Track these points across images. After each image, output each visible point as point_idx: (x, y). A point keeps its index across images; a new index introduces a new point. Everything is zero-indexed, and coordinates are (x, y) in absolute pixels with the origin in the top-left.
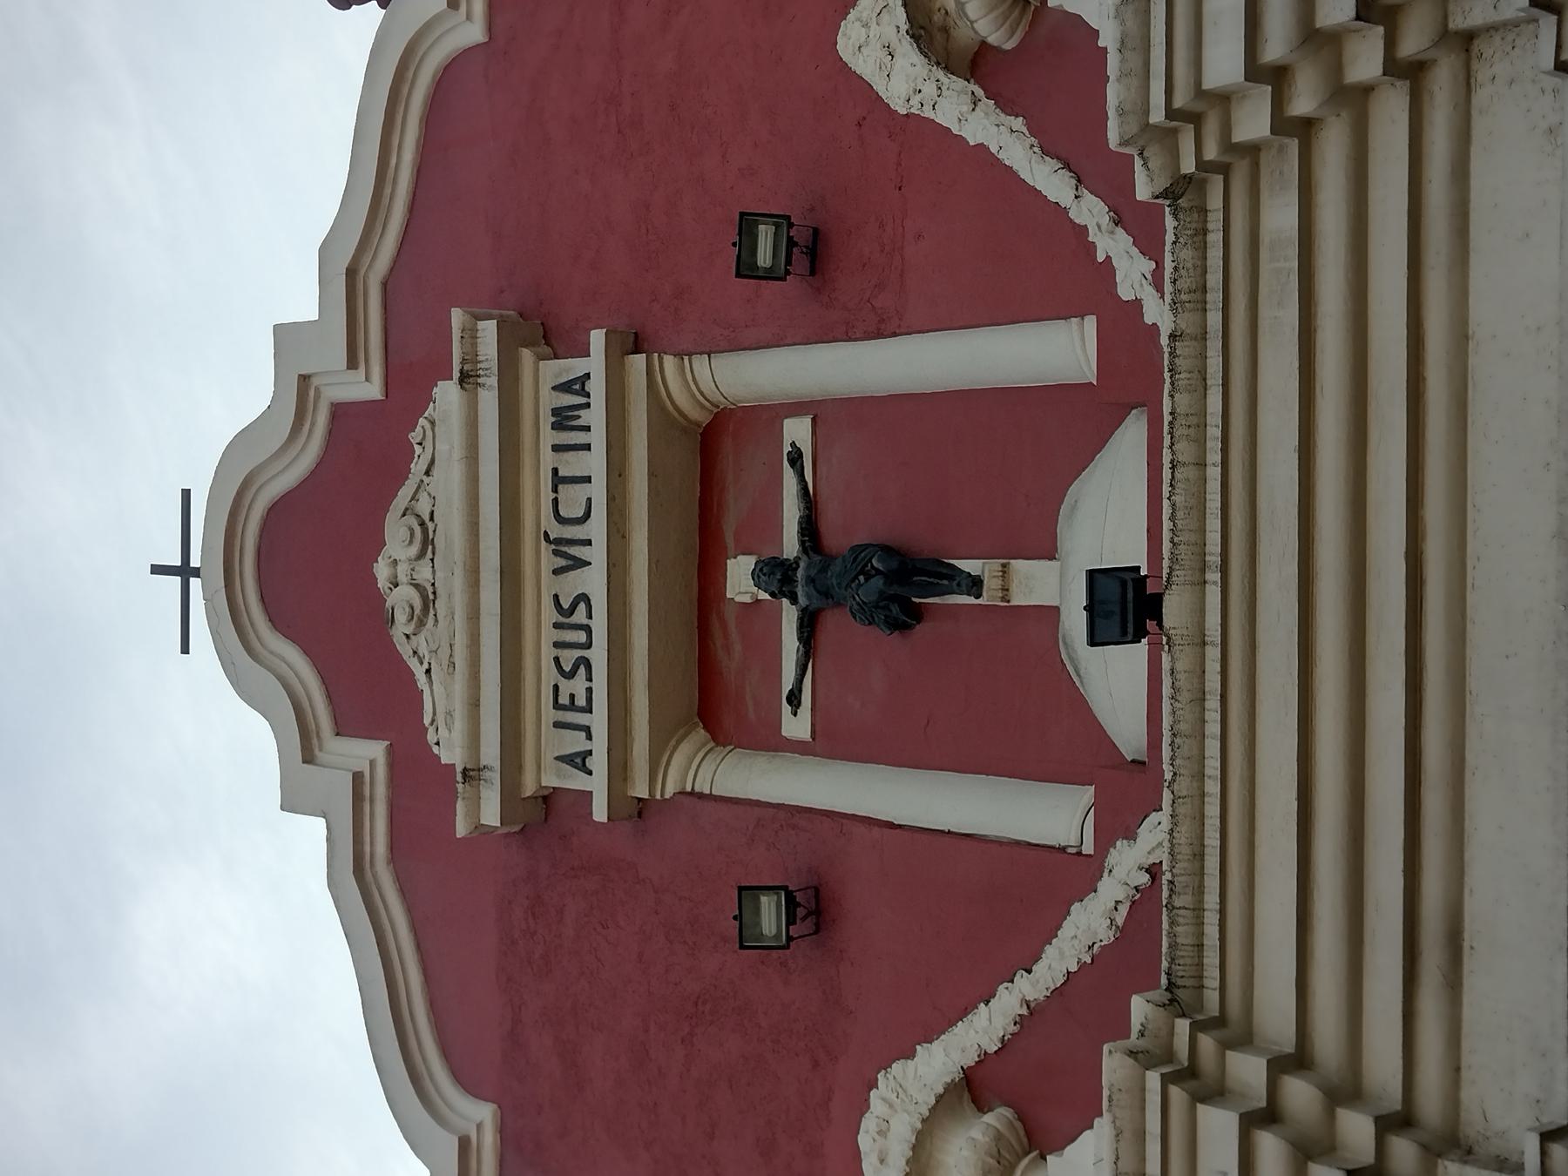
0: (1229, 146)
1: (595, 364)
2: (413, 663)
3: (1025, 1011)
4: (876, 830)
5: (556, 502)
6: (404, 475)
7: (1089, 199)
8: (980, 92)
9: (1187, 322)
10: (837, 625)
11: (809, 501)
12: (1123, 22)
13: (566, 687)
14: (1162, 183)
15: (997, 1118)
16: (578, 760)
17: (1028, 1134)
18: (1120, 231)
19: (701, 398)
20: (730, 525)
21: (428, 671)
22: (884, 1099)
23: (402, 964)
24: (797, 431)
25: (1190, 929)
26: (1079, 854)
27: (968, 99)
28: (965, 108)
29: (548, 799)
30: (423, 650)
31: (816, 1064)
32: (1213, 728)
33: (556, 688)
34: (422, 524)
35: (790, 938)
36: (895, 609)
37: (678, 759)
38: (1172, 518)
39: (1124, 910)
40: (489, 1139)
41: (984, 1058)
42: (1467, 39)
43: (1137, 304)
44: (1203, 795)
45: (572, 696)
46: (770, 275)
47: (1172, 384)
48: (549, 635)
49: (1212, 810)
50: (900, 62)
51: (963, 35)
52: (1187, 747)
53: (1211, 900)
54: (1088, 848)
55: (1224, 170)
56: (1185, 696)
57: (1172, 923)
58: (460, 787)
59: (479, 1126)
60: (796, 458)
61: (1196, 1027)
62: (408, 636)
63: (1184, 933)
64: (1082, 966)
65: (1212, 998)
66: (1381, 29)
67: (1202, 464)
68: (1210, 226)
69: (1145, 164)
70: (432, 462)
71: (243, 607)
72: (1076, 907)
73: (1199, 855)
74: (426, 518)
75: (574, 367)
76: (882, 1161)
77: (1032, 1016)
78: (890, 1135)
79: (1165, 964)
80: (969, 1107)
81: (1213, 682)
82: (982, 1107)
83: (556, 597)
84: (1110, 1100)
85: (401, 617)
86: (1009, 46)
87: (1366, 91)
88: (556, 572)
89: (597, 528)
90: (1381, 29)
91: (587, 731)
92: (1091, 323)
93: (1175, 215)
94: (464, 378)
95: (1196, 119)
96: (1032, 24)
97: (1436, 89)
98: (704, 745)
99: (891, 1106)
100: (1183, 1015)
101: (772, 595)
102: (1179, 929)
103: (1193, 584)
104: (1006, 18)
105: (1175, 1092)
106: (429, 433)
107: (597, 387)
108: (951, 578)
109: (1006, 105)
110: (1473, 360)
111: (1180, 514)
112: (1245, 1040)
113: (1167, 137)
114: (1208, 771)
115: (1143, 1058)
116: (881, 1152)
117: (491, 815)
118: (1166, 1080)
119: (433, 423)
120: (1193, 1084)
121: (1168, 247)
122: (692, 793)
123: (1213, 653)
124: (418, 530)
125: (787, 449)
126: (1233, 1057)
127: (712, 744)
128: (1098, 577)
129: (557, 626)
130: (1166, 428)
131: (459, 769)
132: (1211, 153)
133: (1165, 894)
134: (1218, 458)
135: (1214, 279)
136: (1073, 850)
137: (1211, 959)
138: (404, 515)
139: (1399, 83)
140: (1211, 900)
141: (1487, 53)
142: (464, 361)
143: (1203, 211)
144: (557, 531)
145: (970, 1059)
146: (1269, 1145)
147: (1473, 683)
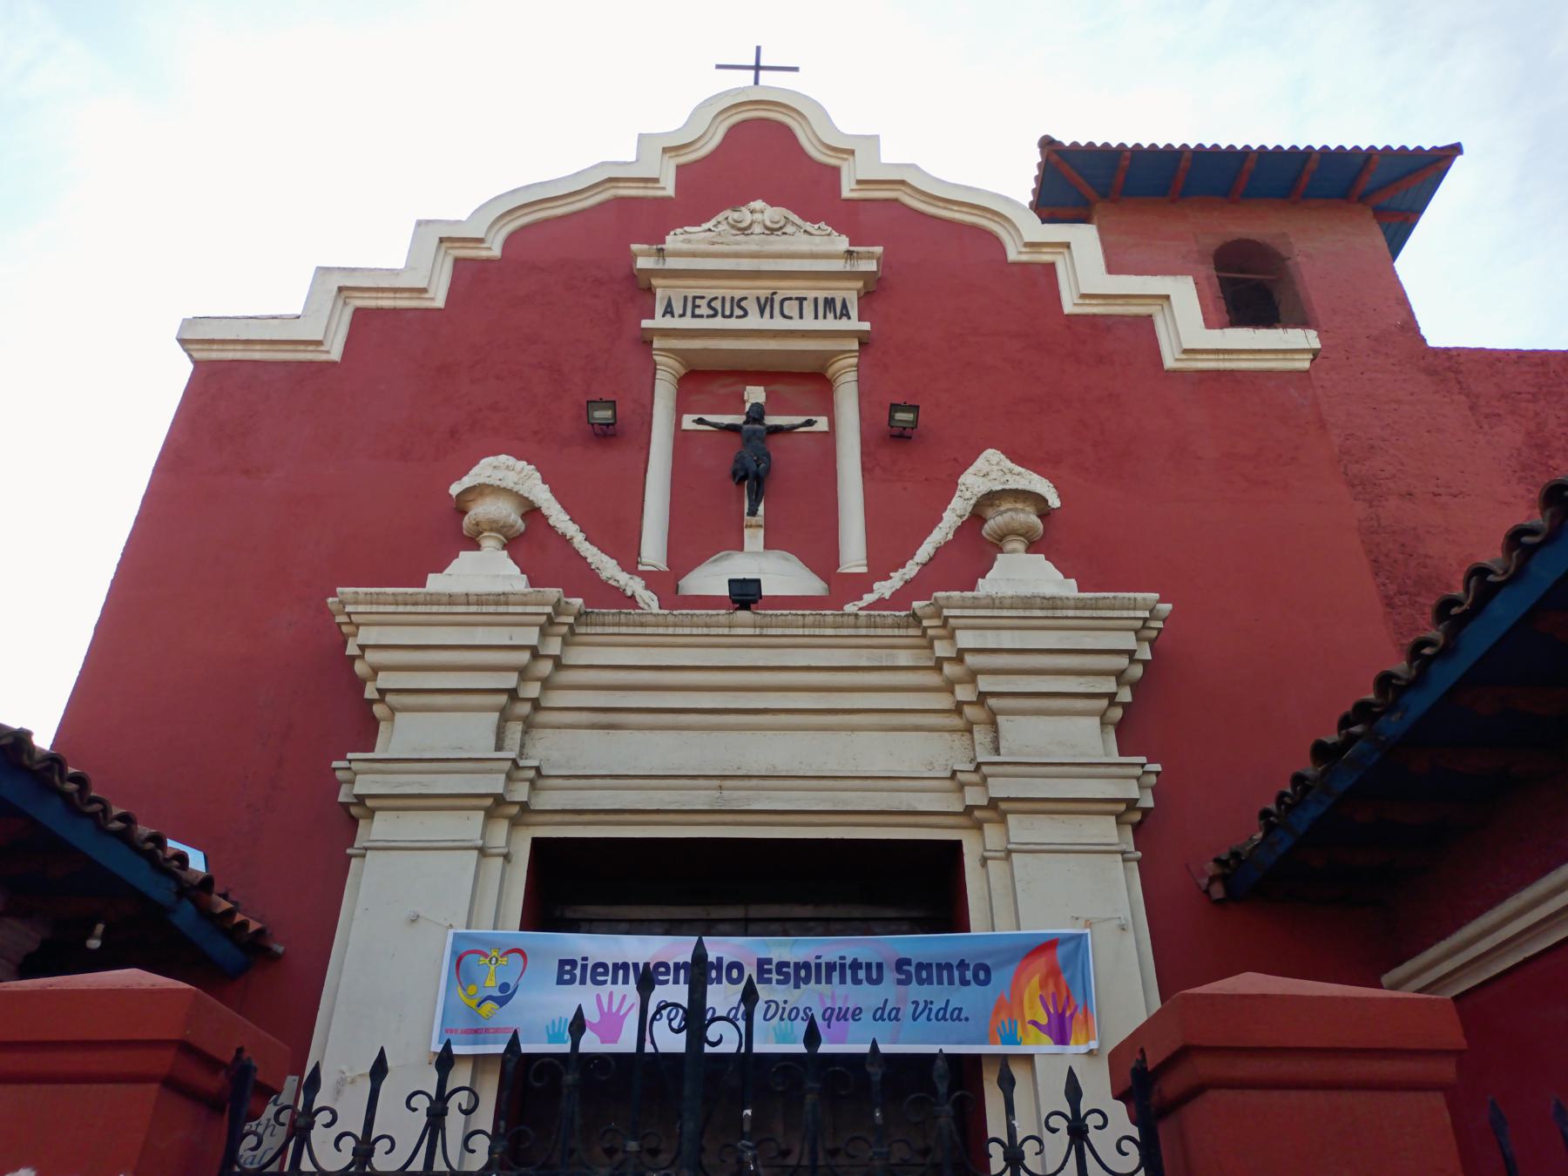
0: (932, 639)
1: (854, 324)
2: (713, 222)
3: (568, 537)
4: (643, 466)
5: (790, 299)
6: (805, 219)
7: (917, 569)
8: (965, 518)
10: (733, 441)
12: (985, 598)
13: (703, 303)
14: (919, 612)
15: (520, 525)
16: (669, 310)
17: (514, 538)
18: (901, 583)
19: (838, 374)
20: (780, 388)
21: (710, 230)
22: (523, 469)
23: (565, 204)
24: (822, 424)
25: (611, 621)
26: (638, 563)
27: (962, 513)
28: (958, 512)
29: (650, 291)
30: (721, 228)
31: (536, 433)
32: (695, 631)
33: (703, 298)
34: (781, 228)
35: (593, 424)
36: (742, 473)
37: (671, 362)
38: (782, 615)
39: (615, 584)
40: (484, 254)
41: (545, 518)
42: (970, 731)
43: (871, 591)
44: (667, 626)
45: (699, 306)
46: (891, 418)
47: (837, 615)
48: (728, 294)
49: (661, 630)
50: (981, 480)
51: (990, 512)
52: (687, 620)
53: (624, 630)
54: (641, 568)
55: (924, 635)
56: (708, 620)
57: (613, 614)
58: (655, 247)
59: (490, 249)
60: (810, 423)
61: (571, 626)
62: (727, 218)
63: (609, 619)
64: (589, 565)
65: (583, 630)
66: (975, 699)
68: (901, 630)
69: (927, 605)
70: (811, 234)
71: (740, 110)
72: (614, 562)
73: (642, 625)
74: (784, 230)
75: (854, 313)
76: (495, 467)
77: (566, 541)
78: (507, 471)
79: (596, 611)
80: (522, 511)
81: (714, 631)
82: (524, 516)
83: (745, 298)
84: (539, 591)
85: (736, 215)
86: (983, 532)
87: (952, 692)
88: (758, 299)
89: (779, 323)
90: (975, 699)
91: (683, 315)
92: (864, 570)
93: (906, 616)
94: (850, 253)
95: (945, 625)
96: (992, 543)
97: (951, 719)
98: (677, 373)
99: (520, 472)
100: (575, 619)
101: (748, 413)
102: (611, 617)
103: (755, 623)
104: (999, 527)
105: (544, 618)
106: (824, 233)
107: (843, 325)
108: (757, 495)
109: (959, 531)
110: (843, 733)
111: (783, 618)
112: (566, 643)
113: (938, 615)
114: (677, 629)
115: (557, 606)
116: (499, 467)
117: (643, 263)
118: (548, 615)
119: (829, 235)
120: (547, 624)
121: (893, 613)
122: (655, 369)
123: (726, 631)
124: (777, 226)
125: (814, 418)
126: (559, 640)
127: (678, 377)
128: (756, 585)
129: (732, 298)
130: (819, 612)
131: (663, 246)
132: (930, 632)
133: (626, 611)
134: (806, 633)
135: (879, 632)
136: (639, 559)
137: (599, 630)
138: (785, 217)
139: (954, 705)
140: (624, 630)
141: (963, 738)
142: (858, 253)
143: (907, 627)
144: (777, 299)
145: (545, 511)
146: (525, 657)
147: (715, 734)
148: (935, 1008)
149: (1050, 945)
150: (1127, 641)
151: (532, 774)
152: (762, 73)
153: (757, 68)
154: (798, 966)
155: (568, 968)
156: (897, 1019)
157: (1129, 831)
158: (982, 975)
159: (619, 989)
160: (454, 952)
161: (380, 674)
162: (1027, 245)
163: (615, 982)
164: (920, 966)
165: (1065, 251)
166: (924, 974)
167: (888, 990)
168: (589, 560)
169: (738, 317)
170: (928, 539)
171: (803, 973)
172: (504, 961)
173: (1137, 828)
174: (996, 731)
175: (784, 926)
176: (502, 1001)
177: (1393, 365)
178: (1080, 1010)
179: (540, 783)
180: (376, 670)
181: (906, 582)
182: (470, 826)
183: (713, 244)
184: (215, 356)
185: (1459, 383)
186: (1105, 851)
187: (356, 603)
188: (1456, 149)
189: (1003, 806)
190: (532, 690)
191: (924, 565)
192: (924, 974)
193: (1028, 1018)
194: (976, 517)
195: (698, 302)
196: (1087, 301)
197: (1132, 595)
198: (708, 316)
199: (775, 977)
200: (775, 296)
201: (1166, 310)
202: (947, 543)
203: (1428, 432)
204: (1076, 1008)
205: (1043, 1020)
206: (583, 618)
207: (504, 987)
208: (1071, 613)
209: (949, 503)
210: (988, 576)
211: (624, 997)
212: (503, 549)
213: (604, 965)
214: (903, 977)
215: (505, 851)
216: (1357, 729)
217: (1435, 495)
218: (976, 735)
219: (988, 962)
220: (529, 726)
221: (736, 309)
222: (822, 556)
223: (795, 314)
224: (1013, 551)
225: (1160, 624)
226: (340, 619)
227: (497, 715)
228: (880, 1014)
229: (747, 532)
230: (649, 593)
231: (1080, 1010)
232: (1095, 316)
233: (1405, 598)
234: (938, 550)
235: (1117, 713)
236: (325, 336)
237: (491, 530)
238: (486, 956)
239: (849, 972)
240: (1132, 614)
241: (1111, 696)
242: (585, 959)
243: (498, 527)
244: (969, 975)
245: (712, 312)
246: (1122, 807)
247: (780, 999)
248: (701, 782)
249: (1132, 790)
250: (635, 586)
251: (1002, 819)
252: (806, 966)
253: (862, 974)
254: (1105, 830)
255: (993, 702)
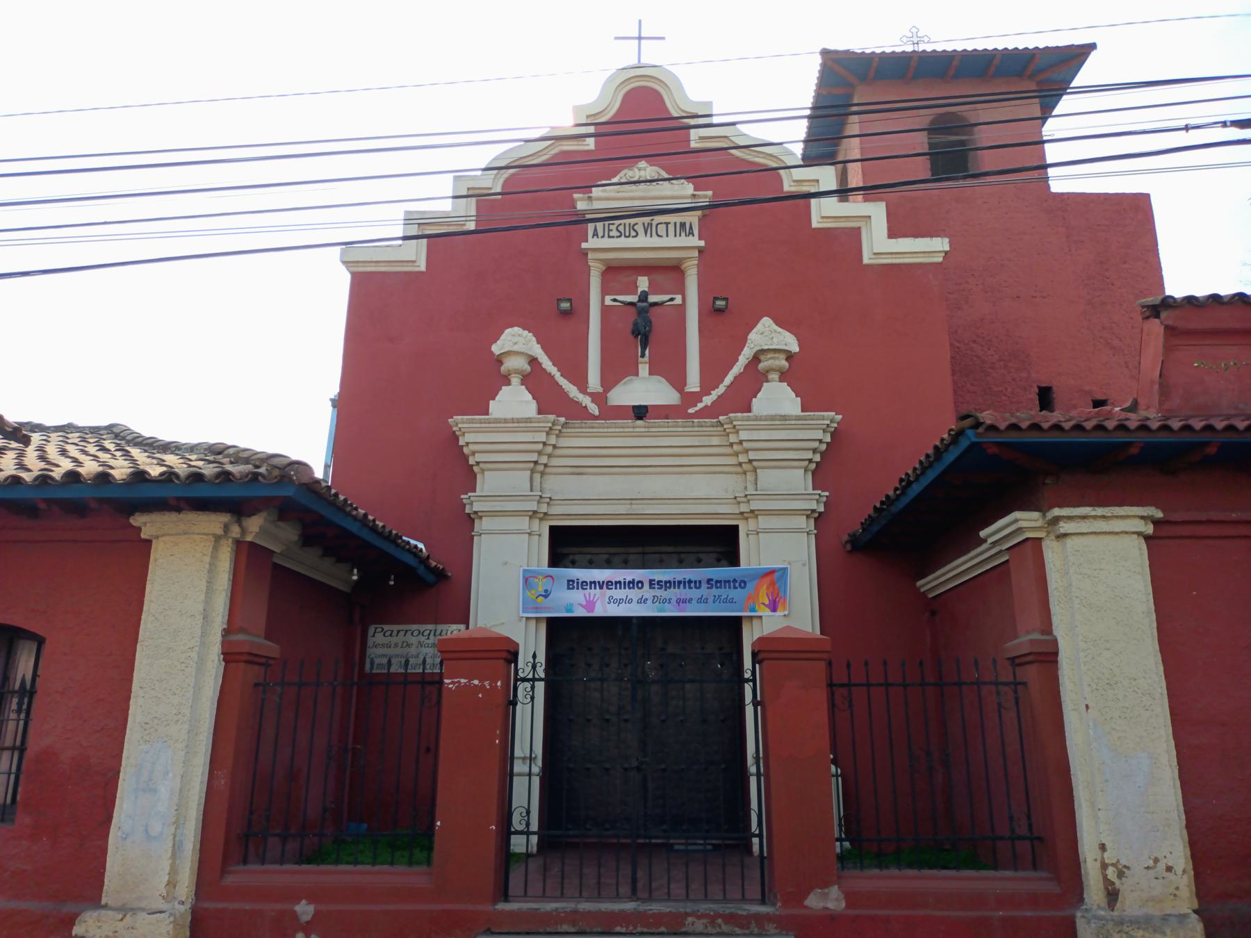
5: (661, 223)
9: (695, 424)
11: (663, 303)
14: (722, 422)
15: (528, 368)
18: (716, 397)
20: (658, 277)
32: (617, 430)
41: (540, 364)
43: (701, 401)
45: (612, 230)
49: (601, 430)
50: (760, 336)
53: (584, 430)
54: (588, 391)
56: (623, 425)
57: (579, 423)
60: (672, 299)
63: (577, 425)
64: (564, 390)
67: (668, 427)
73: (592, 428)
77: (551, 377)
81: (626, 430)
83: (637, 224)
88: (644, 224)
91: (603, 237)
92: (698, 389)
94: (694, 196)
105: (548, 429)
109: (746, 367)
115: (554, 424)
117: (581, 206)
123: (631, 430)
126: (555, 436)
129: (630, 224)
132: (727, 430)
137: (573, 430)
148: (722, 598)
149: (772, 572)
150: (819, 435)
151: (548, 500)
152: (643, 41)
153: (640, 38)
154: (666, 582)
155: (571, 583)
156: (706, 602)
157: (812, 522)
158: (743, 585)
159: (593, 591)
160: (524, 577)
161: (476, 455)
162: (794, 181)
163: (591, 588)
164: (717, 582)
165: (816, 184)
166: (719, 585)
167: (704, 591)
168: (563, 387)
169: (633, 237)
170: (731, 372)
171: (668, 585)
172: (544, 580)
173: (816, 520)
174: (756, 475)
175: (661, 564)
176: (546, 596)
177: (1027, 207)
178: (783, 598)
179: (551, 502)
180: (474, 453)
181: (719, 397)
182: (524, 523)
183: (618, 192)
184: (360, 269)
185: (1064, 219)
186: (798, 531)
187: (463, 423)
188: (1093, 46)
189: (756, 513)
190: (544, 460)
191: (728, 387)
192: (719, 585)
193: (761, 602)
194: (756, 359)
195: (611, 227)
196: (825, 220)
197: (822, 413)
198: (617, 237)
199: (656, 586)
200: (653, 222)
201: (868, 223)
202: (740, 374)
203: (1039, 254)
204: (781, 598)
205: (767, 602)
206: (565, 426)
207: (546, 591)
208: (793, 422)
209: (742, 350)
210: (759, 396)
211: (595, 595)
212: (522, 384)
213: (586, 582)
214: (709, 586)
215: (539, 533)
216: (885, 507)
217: (1033, 297)
218: (748, 477)
219: (745, 580)
220: (542, 474)
221: (632, 231)
222: (678, 381)
223: (663, 233)
224: (773, 380)
225: (836, 425)
226: (455, 429)
227: (529, 472)
228: (700, 600)
229: (640, 366)
230: (594, 404)
231: (783, 598)
232: (829, 229)
233: (1002, 363)
234: (736, 378)
235: (813, 466)
236: (417, 257)
237: (515, 373)
238: (537, 578)
239: (687, 584)
240: (822, 422)
241: (810, 461)
242: (578, 579)
243: (517, 372)
244: (737, 585)
245: (619, 234)
246: (809, 512)
247: (659, 595)
248: (622, 502)
249: (814, 506)
250: (586, 401)
251: (756, 517)
252: (670, 582)
253: (692, 585)
254: (801, 522)
255: (755, 464)
